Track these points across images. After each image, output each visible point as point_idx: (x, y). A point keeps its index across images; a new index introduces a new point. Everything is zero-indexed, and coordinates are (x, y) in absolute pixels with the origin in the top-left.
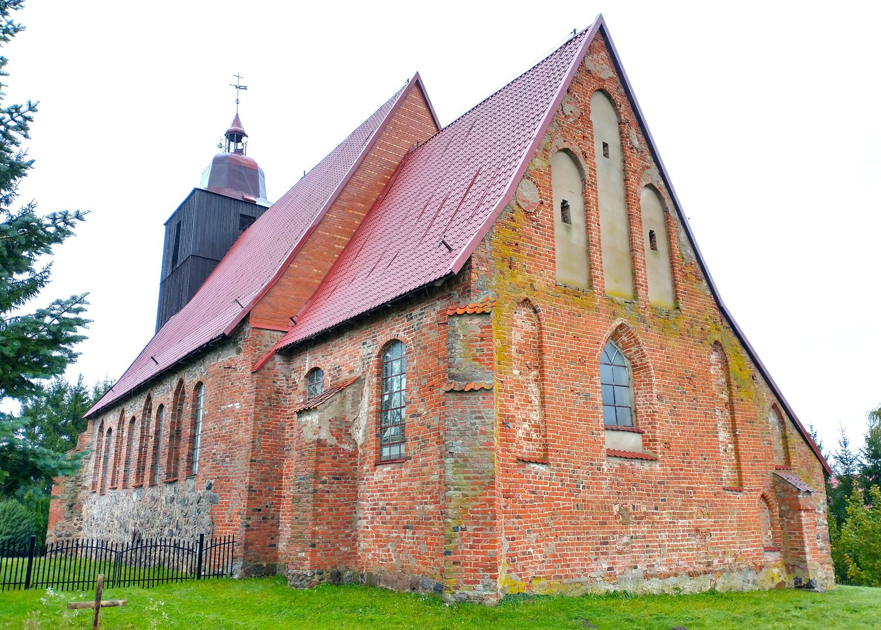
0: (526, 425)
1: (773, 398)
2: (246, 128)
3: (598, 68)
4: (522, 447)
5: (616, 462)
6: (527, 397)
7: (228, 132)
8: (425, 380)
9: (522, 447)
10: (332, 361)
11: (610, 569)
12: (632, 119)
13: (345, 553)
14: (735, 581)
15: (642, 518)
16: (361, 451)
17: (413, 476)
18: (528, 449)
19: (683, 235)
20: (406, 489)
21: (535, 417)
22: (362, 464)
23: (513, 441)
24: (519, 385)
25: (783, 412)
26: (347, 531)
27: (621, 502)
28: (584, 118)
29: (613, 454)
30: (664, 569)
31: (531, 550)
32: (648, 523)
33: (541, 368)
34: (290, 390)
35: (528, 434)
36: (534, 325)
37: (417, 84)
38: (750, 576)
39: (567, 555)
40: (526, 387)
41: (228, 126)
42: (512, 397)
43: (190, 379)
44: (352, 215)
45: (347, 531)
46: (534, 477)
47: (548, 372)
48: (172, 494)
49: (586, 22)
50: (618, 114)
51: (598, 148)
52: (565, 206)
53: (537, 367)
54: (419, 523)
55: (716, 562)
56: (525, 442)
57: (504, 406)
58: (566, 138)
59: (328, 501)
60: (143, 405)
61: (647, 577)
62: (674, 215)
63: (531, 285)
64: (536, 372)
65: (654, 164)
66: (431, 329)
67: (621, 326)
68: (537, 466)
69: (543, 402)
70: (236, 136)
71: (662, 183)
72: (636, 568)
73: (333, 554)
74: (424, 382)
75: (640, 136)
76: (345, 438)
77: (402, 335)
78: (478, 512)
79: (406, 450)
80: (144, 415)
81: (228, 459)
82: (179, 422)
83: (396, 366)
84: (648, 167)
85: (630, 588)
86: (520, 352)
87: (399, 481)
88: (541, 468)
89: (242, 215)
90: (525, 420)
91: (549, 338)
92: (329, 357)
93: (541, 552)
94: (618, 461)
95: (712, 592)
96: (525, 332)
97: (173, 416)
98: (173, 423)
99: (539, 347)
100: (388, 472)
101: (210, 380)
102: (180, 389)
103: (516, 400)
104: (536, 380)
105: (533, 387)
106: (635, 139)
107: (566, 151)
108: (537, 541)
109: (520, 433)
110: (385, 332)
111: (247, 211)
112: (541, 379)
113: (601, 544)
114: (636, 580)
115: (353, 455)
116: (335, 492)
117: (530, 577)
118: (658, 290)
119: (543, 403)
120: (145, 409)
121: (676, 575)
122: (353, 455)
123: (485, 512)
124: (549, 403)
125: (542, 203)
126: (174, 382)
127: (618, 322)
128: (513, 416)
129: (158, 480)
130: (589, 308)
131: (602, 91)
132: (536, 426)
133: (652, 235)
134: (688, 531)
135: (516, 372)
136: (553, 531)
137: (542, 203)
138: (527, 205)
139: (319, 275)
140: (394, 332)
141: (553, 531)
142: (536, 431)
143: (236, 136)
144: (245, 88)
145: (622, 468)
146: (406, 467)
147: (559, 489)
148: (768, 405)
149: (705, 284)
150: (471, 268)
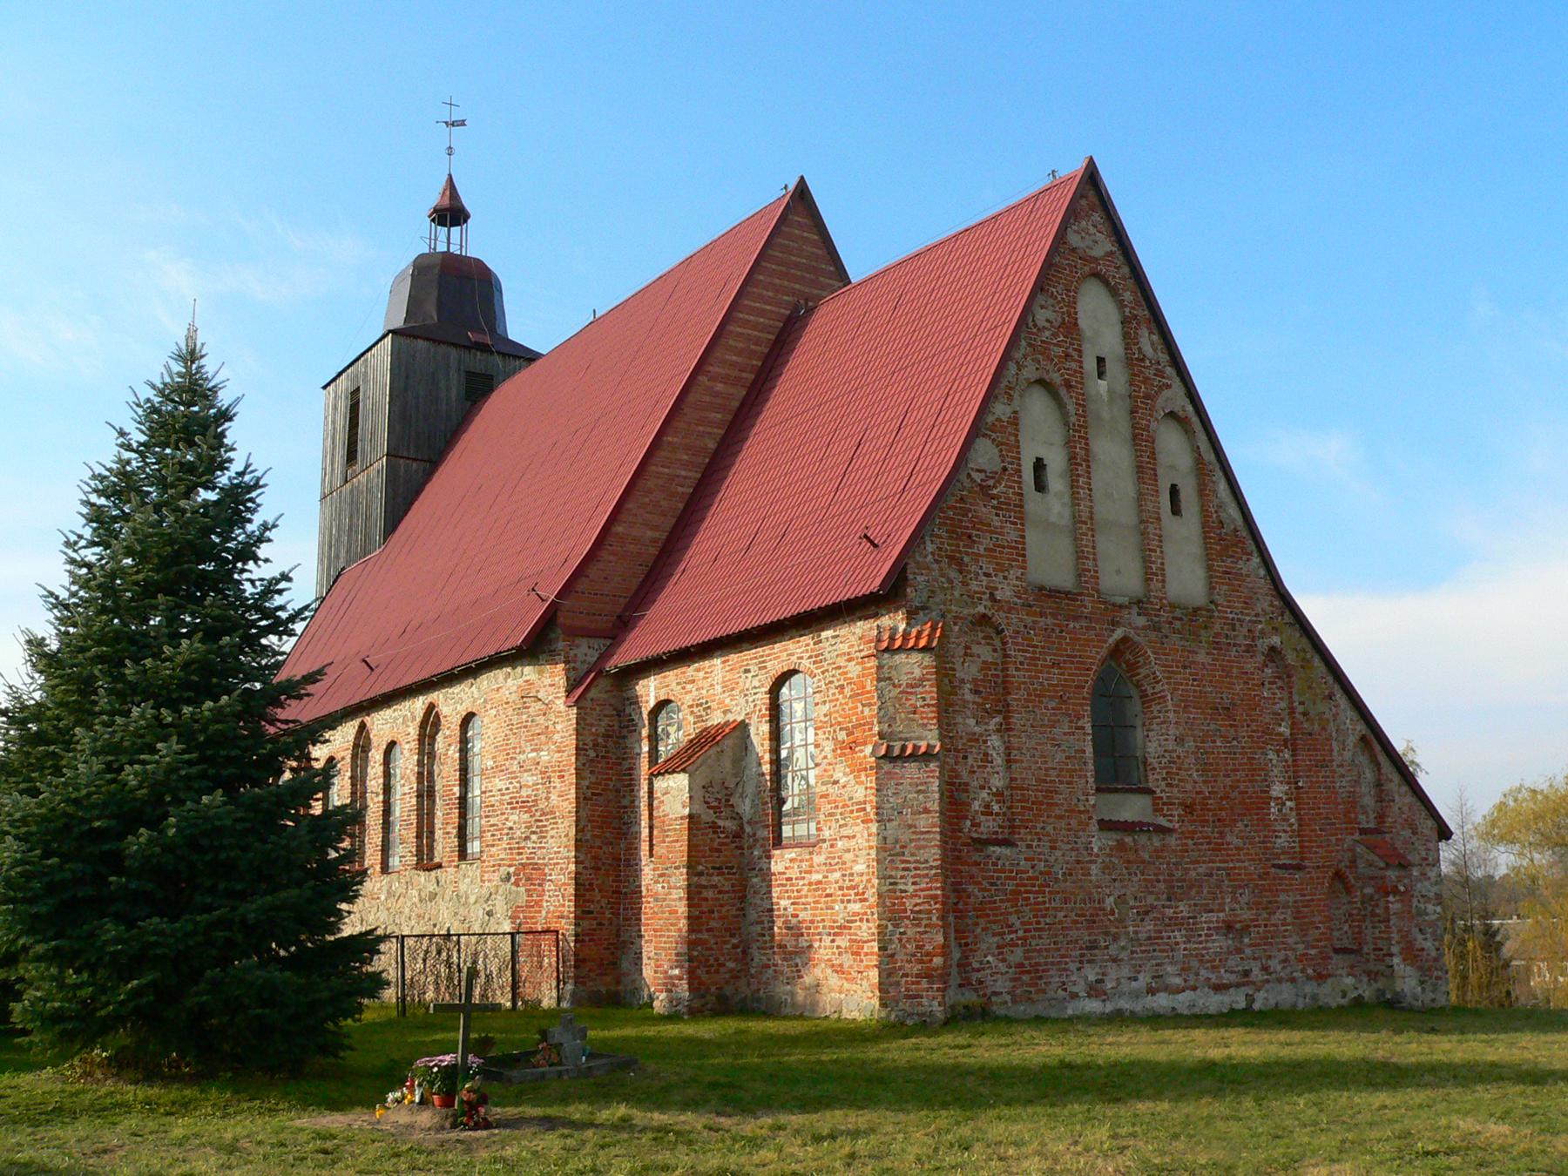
0: (984, 794)
1: (1361, 728)
2: (467, 202)
3: (1088, 242)
4: (978, 825)
5: (1110, 839)
6: (986, 754)
7: (435, 211)
8: (844, 733)
9: (978, 825)
10: (695, 693)
11: (1098, 981)
12: (1143, 310)
13: (732, 970)
14: (1285, 995)
15: (1147, 913)
16: (748, 829)
17: (829, 867)
18: (988, 826)
19: (1222, 486)
20: (820, 882)
21: (997, 782)
22: (750, 848)
23: (966, 817)
24: (974, 738)
25: (1377, 748)
26: (735, 941)
27: (1117, 893)
28: (1070, 327)
29: (1106, 825)
30: (1178, 981)
31: (989, 958)
32: (1156, 919)
33: (1006, 712)
34: (625, 732)
35: (987, 806)
36: (995, 651)
37: (801, 196)
38: (1309, 988)
39: (1038, 964)
40: (985, 742)
41: (433, 197)
42: (965, 757)
43: (451, 703)
44: (701, 435)
45: (735, 941)
46: (995, 864)
47: (1016, 720)
48: (432, 887)
49: (1072, 166)
50: (1121, 305)
51: (1090, 365)
52: (1039, 466)
53: (1000, 712)
54: (840, 927)
55: (1256, 971)
56: (983, 818)
57: (953, 770)
58: (1038, 350)
59: (706, 899)
60: (351, 738)
61: (1151, 991)
62: (1210, 457)
63: (992, 595)
64: (998, 719)
65: (1177, 380)
66: (849, 660)
67: (1125, 639)
68: (998, 849)
69: (1008, 761)
70: (451, 214)
71: (1190, 408)
72: (1136, 979)
73: (717, 972)
74: (842, 736)
75: (1155, 338)
76: (726, 812)
77: (806, 664)
78: (920, 912)
79: (819, 829)
80: (354, 757)
81: (534, 837)
82: (431, 773)
83: (798, 707)
84: (1168, 386)
85: (1125, 1004)
86: (976, 692)
87: (809, 872)
88: (1006, 851)
89: (468, 373)
90: (982, 788)
91: (1017, 669)
92: (689, 687)
93: (1004, 960)
94: (1116, 836)
95: (1248, 1010)
96: (984, 662)
97: (420, 763)
98: (420, 774)
99: (1004, 682)
100: (792, 860)
101: (494, 712)
102: (430, 724)
103: (970, 761)
104: (998, 731)
105: (995, 741)
106: (1147, 342)
107: (1041, 382)
108: (998, 947)
109: (976, 806)
110: (780, 654)
111: (477, 362)
112: (1005, 729)
113: (1088, 948)
114: (1136, 995)
115: (738, 835)
116: (715, 887)
117: (988, 992)
118: (1186, 577)
119: (1009, 761)
120: (356, 746)
121: (1194, 989)
122: (738, 835)
123: (929, 912)
124: (1016, 761)
125: (1005, 469)
126: (418, 705)
127: (1119, 633)
128: (966, 784)
129: (395, 862)
130: (1076, 618)
131: (1095, 275)
132: (999, 794)
133: (1174, 491)
134: (1217, 928)
135: (972, 722)
136: (1021, 933)
137: (1005, 469)
138: (982, 476)
139: (654, 540)
140: (794, 658)
141: (1021, 933)
142: (998, 802)
143: (451, 214)
144: (462, 123)
145: (1121, 846)
146: (819, 853)
147: (1029, 878)
148: (1351, 740)
149: (1256, 560)
150: (906, 579)
